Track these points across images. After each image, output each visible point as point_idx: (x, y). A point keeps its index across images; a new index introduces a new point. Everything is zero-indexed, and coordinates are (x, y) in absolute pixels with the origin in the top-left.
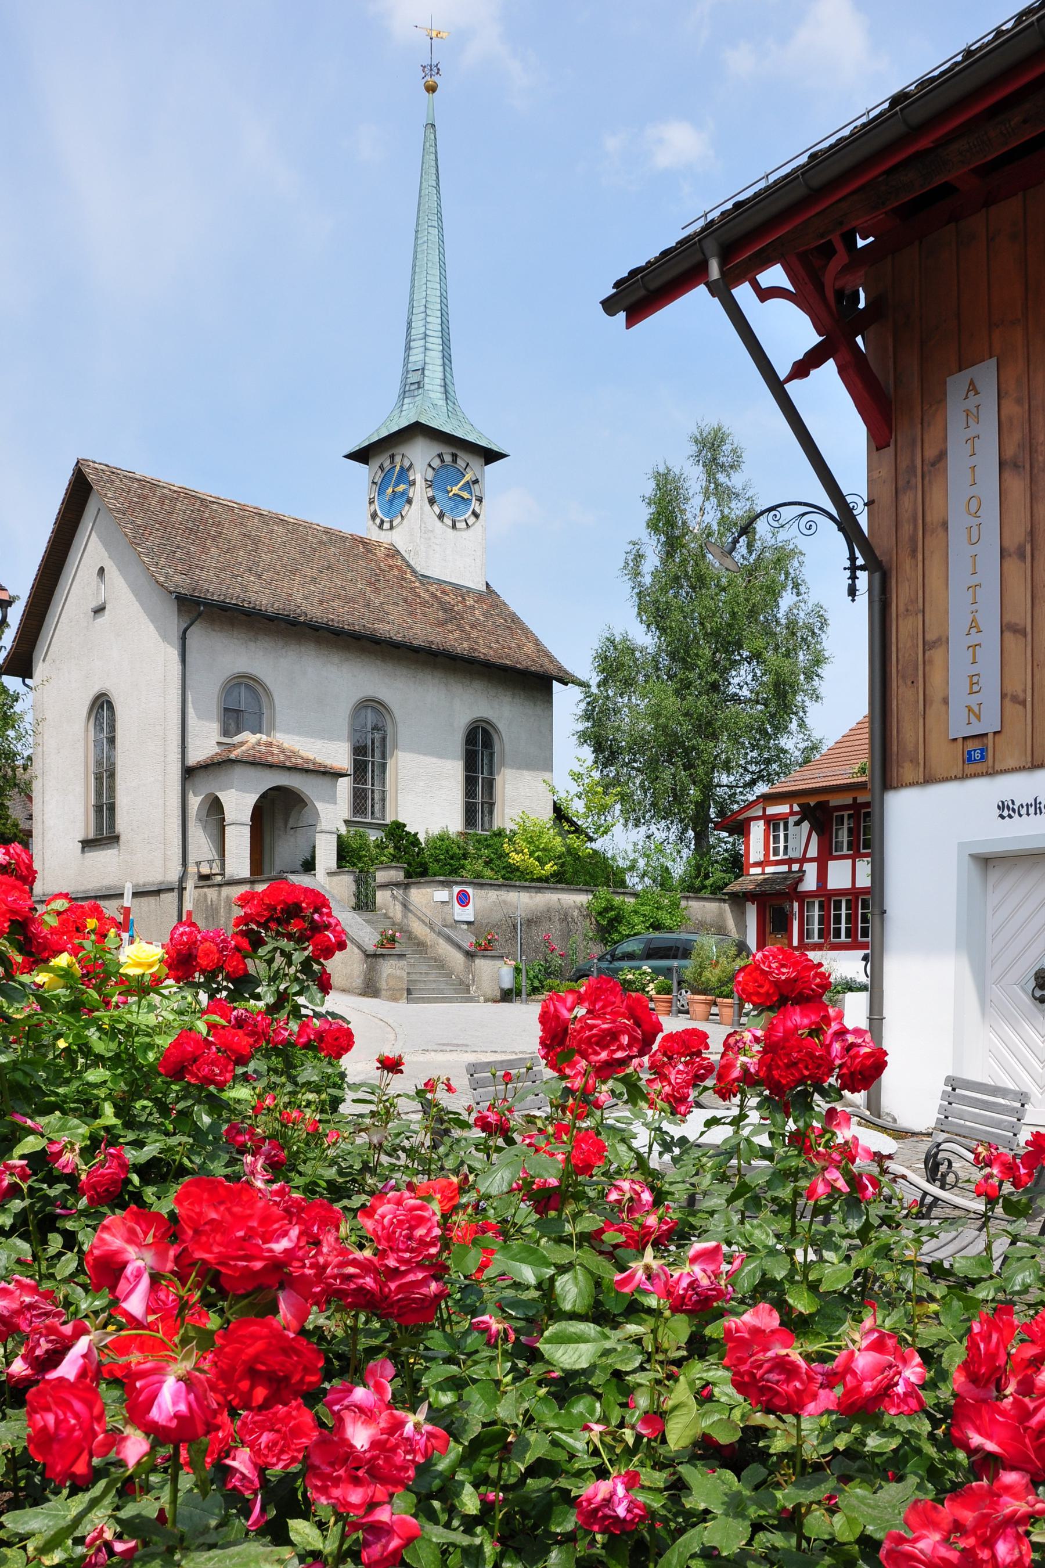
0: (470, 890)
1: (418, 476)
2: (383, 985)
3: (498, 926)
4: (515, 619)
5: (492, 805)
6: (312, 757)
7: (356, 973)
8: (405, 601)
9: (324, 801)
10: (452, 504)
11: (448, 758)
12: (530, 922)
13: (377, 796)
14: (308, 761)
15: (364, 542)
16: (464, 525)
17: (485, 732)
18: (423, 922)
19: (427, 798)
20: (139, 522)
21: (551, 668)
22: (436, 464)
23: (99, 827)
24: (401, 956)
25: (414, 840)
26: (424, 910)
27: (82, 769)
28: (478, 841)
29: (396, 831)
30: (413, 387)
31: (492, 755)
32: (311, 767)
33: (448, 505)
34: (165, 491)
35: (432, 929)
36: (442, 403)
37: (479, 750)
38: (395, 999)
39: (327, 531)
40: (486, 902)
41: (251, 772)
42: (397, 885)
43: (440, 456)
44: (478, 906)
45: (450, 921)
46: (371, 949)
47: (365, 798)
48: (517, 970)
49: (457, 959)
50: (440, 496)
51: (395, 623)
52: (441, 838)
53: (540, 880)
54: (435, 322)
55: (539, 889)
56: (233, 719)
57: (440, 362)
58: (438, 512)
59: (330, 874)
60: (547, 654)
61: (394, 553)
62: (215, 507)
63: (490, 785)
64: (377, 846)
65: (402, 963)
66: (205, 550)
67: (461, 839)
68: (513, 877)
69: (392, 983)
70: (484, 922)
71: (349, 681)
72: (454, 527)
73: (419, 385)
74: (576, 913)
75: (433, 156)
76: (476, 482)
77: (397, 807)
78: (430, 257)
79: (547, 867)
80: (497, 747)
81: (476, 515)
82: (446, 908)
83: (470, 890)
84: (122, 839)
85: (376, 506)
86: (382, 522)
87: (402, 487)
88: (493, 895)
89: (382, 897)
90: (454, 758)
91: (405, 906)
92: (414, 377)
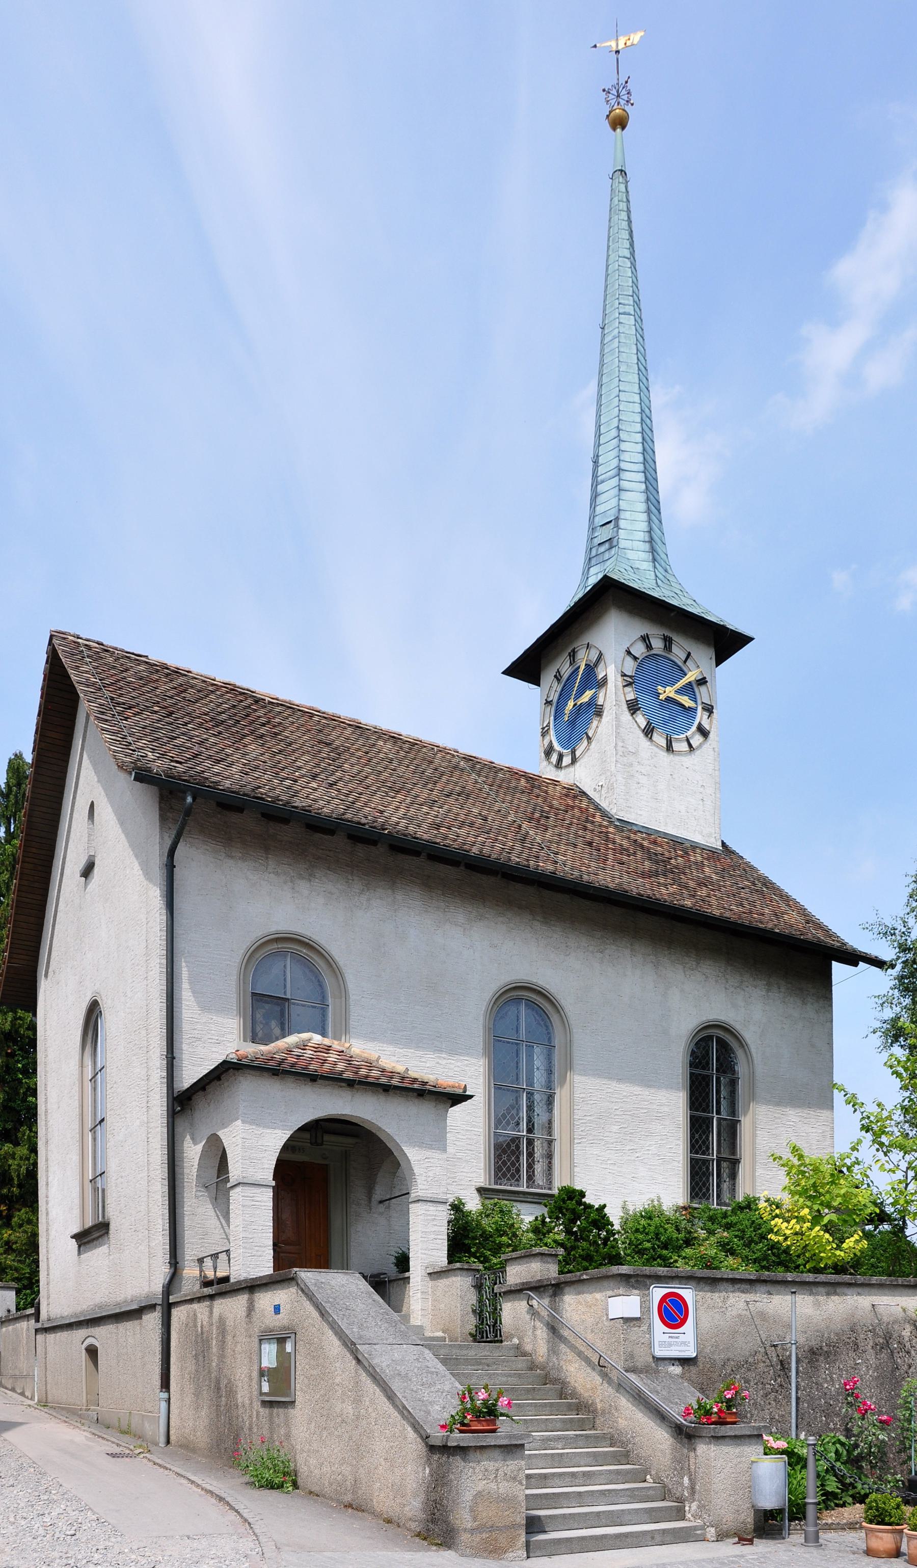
0: (688, 1294)
1: (610, 671)
2: (463, 1518)
3: (748, 1365)
4: (767, 883)
5: (734, 1163)
6: (400, 1068)
8: (590, 844)
9: (421, 1145)
10: (666, 714)
11: (659, 1088)
12: (816, 1354)
13: (538, 1152)
14: (392, 1074)
15: (533, 781)
16: (684, 746)
17: (724, 1046)
18: (588, 1361)
19: (626, 1154)
22: (639, 650)
24: (513, 1449)
25: (599, 1218)
26: (590, 1337)
27: (76, 1125)
28: (712, 1219)
29: (570, 1205)
30: (602, 549)
31: (733, 1083)
32: (395, 1082)
33: (660, 715)
35: (605, 1376)
36: (647, 566)
37: (713, 1075)
38: (493, 1550)
39: (468, 759)
40: (721, 1317)
41: (273, 1089)
42: (538, 1288)
43: (645, 639)
44: (705, 1324)
45: (643, 1359)
46: (438, 1436)
47: (517, 1152)
48: (794, 1460)
49: (657, 1440)
50: (646, 701)
51: (569, 861)
52: (648, 1215)
53: (839, 1268)
54: (633, 450)
55: (833, 1288)
56: (267, 1009)
57: (642, 507)
58: (643, 723)
59: (435, 1275)
60: (819, 926)
61: (575, 794)
63: (731, 1130)
64: (536, 1230)
65: (513, 1465)
67: (682, 1217)
68: (777, 1265)
69: (487, 1513)
70: (719, 1358)
71: (487, 952)
72: (669, 748)
73: (610, 542)
74: (906, 1333)
75: (624, 215)
76: (702, 682)
77: (572, 1166)
78: (623, 357)
79: (849, 1243)
80: (741, 1069)
81: (703, 732)
82: (636, 1333)
83: (688, 1294)
85: (552, 736)
86: (561, 757)
87: (588, 695)
88: (737, 1302)
89: (512, 1313)
90: (669, 1087)
91: (553, 1329)
92: (603, 534)
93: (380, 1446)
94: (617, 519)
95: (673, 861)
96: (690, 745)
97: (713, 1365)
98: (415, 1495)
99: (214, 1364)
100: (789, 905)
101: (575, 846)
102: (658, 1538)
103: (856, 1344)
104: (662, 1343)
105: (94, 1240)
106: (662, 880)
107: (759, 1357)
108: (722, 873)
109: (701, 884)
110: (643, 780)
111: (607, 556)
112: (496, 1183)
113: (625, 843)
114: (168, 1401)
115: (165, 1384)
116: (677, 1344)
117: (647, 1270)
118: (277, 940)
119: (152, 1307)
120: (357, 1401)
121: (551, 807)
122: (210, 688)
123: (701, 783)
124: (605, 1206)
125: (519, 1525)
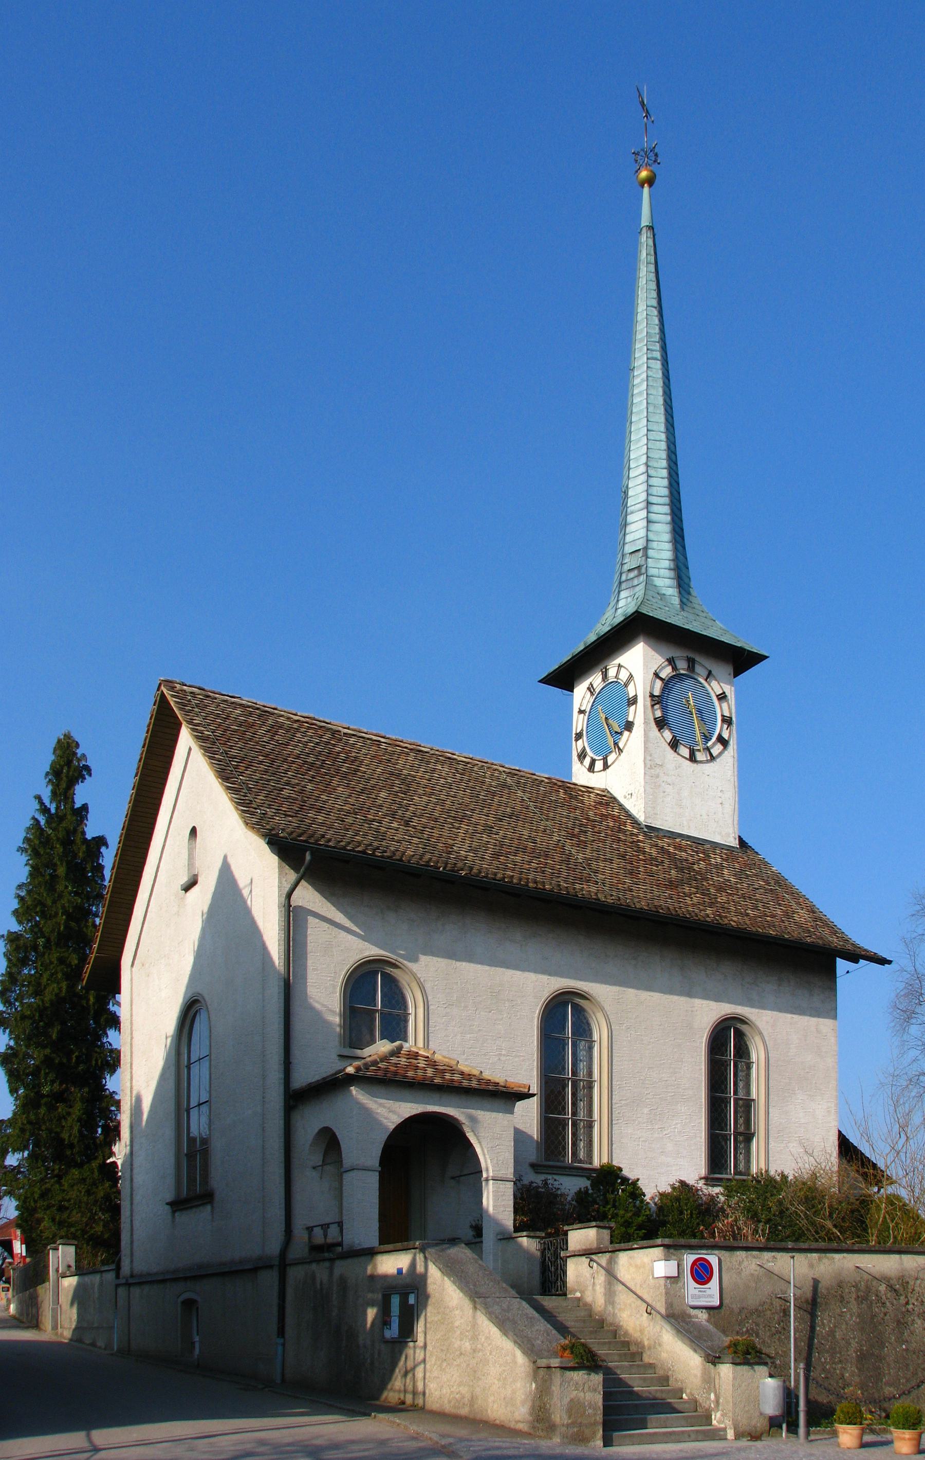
0: (713, 1259)
4: (779, 881)
6: (476, 1072)
7: (520, 1396)
8: (623, 857)
20: (234, 752)
21: (835, 941)
23: (191, 1180)
25: (634, 1191)
30: (632, 575)
32: (474, 1084)
34: (281, 720)
39: (512, 774)
43: (671, 661)
51: (606, 883)
60: (827, 924)
61: (607, 800)
62: (352, 741)
66: (329, 789)
84: (217, 1197)
86: (593, 762)
88: (748, 1264)
93: (494, 1370)
94: (646, 549)
95: (695, 867)
96: (711, 755)
97: (732, 1311)
98: (523, 1403)
99: (334, 1314)
100: (799, 904)
101: (611, 861)
102: (693, 1436)
103: (842, 1297)
104: (694, 1296)
105: (192, 1207)
106: (687, 889)
107: (766, 1306)
108: (740, 875)
109: (720, 889)
110: (669, 789)
111: (636, 582)
112: (546, 1160)
113: (654, 852)
114: (284, 1345)
115: (281, 1332)
116: (704, 1297)
117: (682, 1241)
118: (369, 961)
119: (271, 1267)
120: (474, 1338)
121: (588, 819)
122: (295, 726)
123: (720, 788)
124: (638, 1180)
125: (595, 1423)
